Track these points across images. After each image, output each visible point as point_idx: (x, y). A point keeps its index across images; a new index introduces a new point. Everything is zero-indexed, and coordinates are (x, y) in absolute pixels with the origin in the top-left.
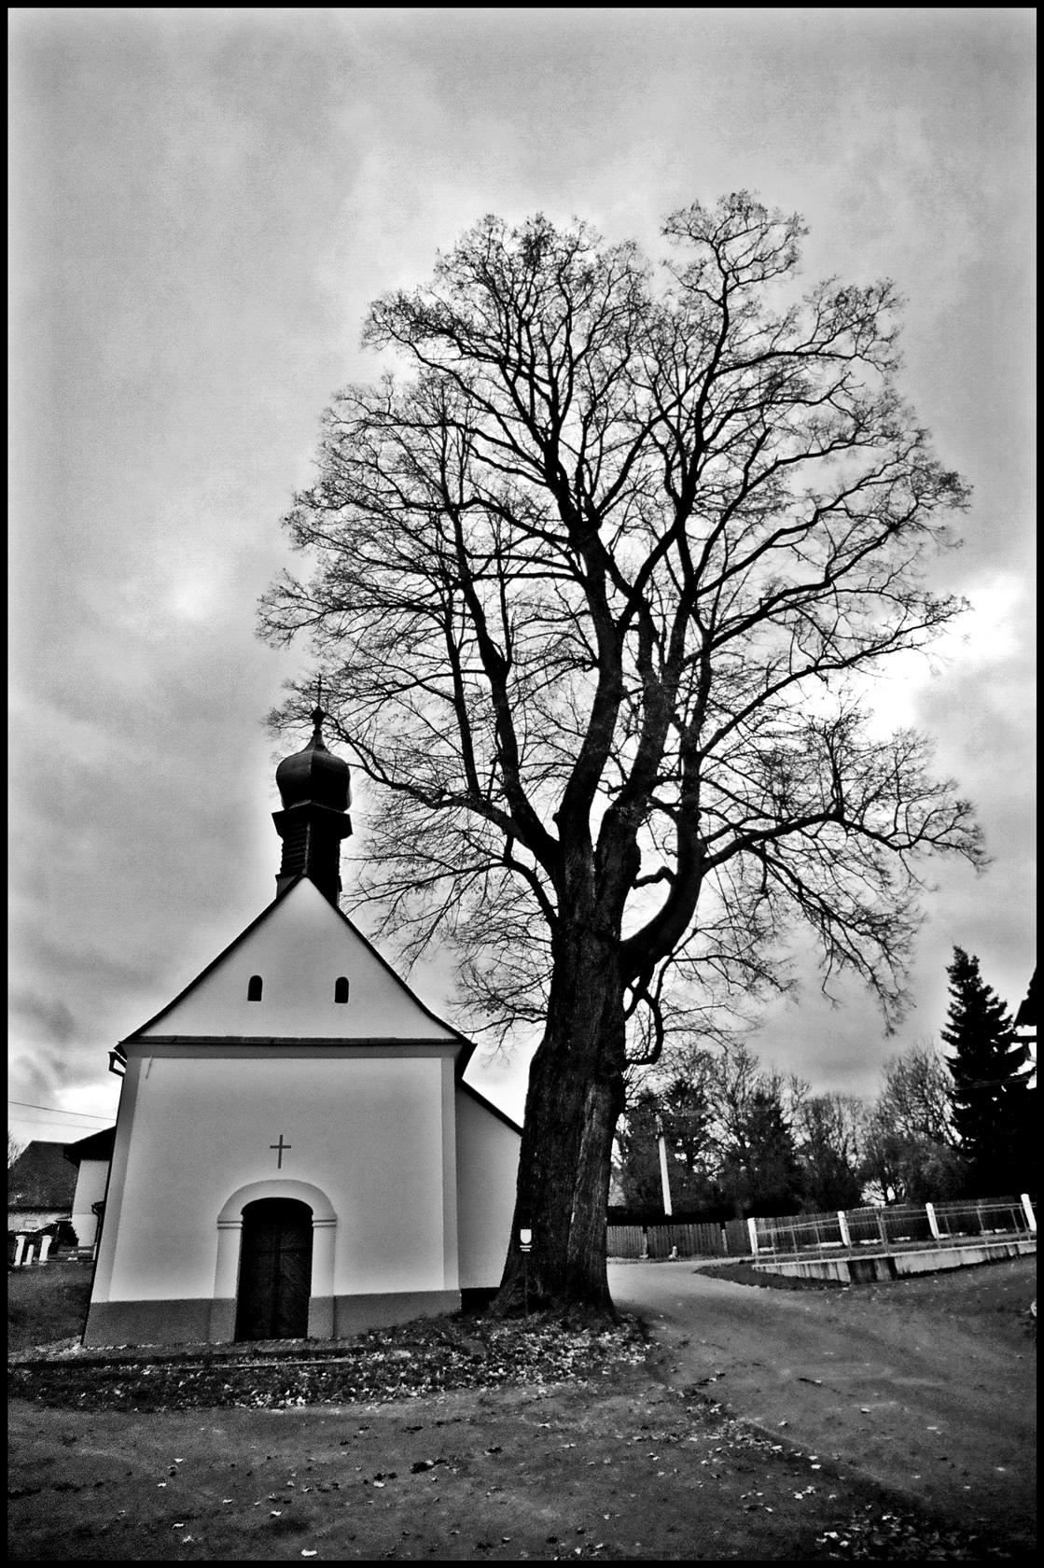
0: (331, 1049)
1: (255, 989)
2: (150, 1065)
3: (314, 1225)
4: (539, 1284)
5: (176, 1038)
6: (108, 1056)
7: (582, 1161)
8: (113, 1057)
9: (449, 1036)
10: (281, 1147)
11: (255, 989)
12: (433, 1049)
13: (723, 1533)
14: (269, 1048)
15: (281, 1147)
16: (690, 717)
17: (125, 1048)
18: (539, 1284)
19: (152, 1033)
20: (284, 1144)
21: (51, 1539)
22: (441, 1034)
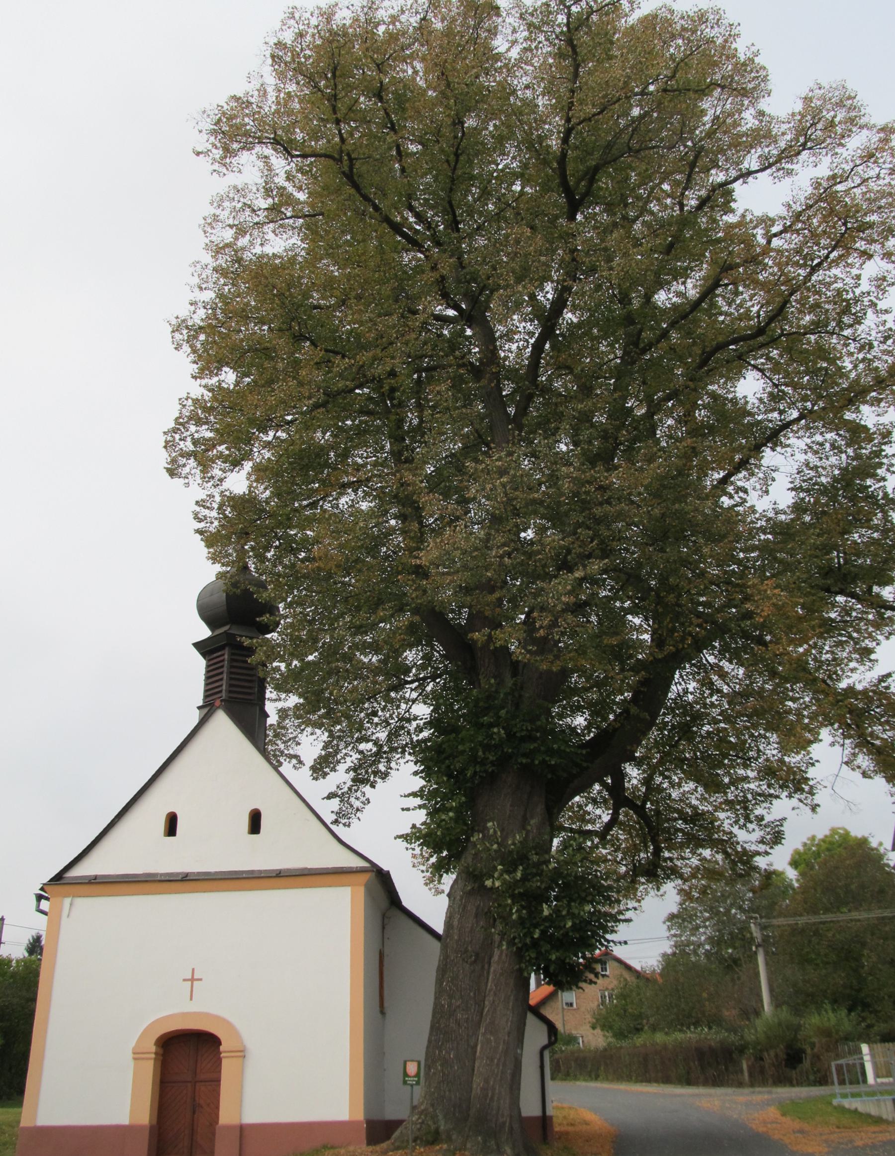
0: (215, 883)
1: (171, 826)
2: (71, 904)
3: (222, 1055)
4: (440, 1117)
5: (96, 877)
6: (34, 898)
7: (490, 990)
8: (39, 898)
9: (366, 865)
10: (192, 980)
11: (171, 826)
12: (344, 878)
13: (586, 805)
14: (181, 883)
15: (192, 980)
16: (694, 203)
17: (46, 888)
18: (440, 1117)
19: (77, 872)
20: (190, 983)
21: (583, 878)
22: (357, 863)
